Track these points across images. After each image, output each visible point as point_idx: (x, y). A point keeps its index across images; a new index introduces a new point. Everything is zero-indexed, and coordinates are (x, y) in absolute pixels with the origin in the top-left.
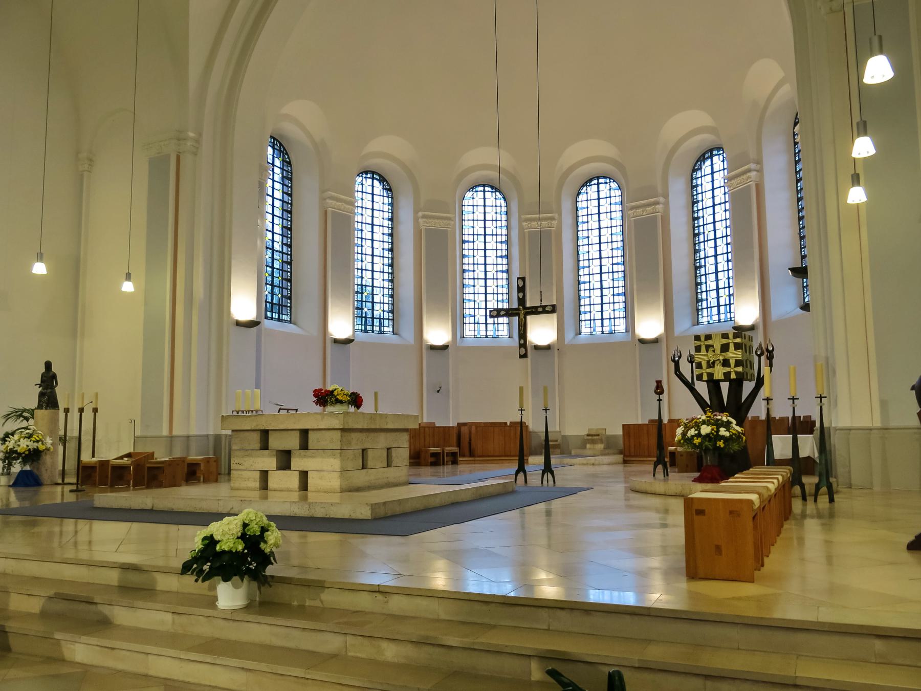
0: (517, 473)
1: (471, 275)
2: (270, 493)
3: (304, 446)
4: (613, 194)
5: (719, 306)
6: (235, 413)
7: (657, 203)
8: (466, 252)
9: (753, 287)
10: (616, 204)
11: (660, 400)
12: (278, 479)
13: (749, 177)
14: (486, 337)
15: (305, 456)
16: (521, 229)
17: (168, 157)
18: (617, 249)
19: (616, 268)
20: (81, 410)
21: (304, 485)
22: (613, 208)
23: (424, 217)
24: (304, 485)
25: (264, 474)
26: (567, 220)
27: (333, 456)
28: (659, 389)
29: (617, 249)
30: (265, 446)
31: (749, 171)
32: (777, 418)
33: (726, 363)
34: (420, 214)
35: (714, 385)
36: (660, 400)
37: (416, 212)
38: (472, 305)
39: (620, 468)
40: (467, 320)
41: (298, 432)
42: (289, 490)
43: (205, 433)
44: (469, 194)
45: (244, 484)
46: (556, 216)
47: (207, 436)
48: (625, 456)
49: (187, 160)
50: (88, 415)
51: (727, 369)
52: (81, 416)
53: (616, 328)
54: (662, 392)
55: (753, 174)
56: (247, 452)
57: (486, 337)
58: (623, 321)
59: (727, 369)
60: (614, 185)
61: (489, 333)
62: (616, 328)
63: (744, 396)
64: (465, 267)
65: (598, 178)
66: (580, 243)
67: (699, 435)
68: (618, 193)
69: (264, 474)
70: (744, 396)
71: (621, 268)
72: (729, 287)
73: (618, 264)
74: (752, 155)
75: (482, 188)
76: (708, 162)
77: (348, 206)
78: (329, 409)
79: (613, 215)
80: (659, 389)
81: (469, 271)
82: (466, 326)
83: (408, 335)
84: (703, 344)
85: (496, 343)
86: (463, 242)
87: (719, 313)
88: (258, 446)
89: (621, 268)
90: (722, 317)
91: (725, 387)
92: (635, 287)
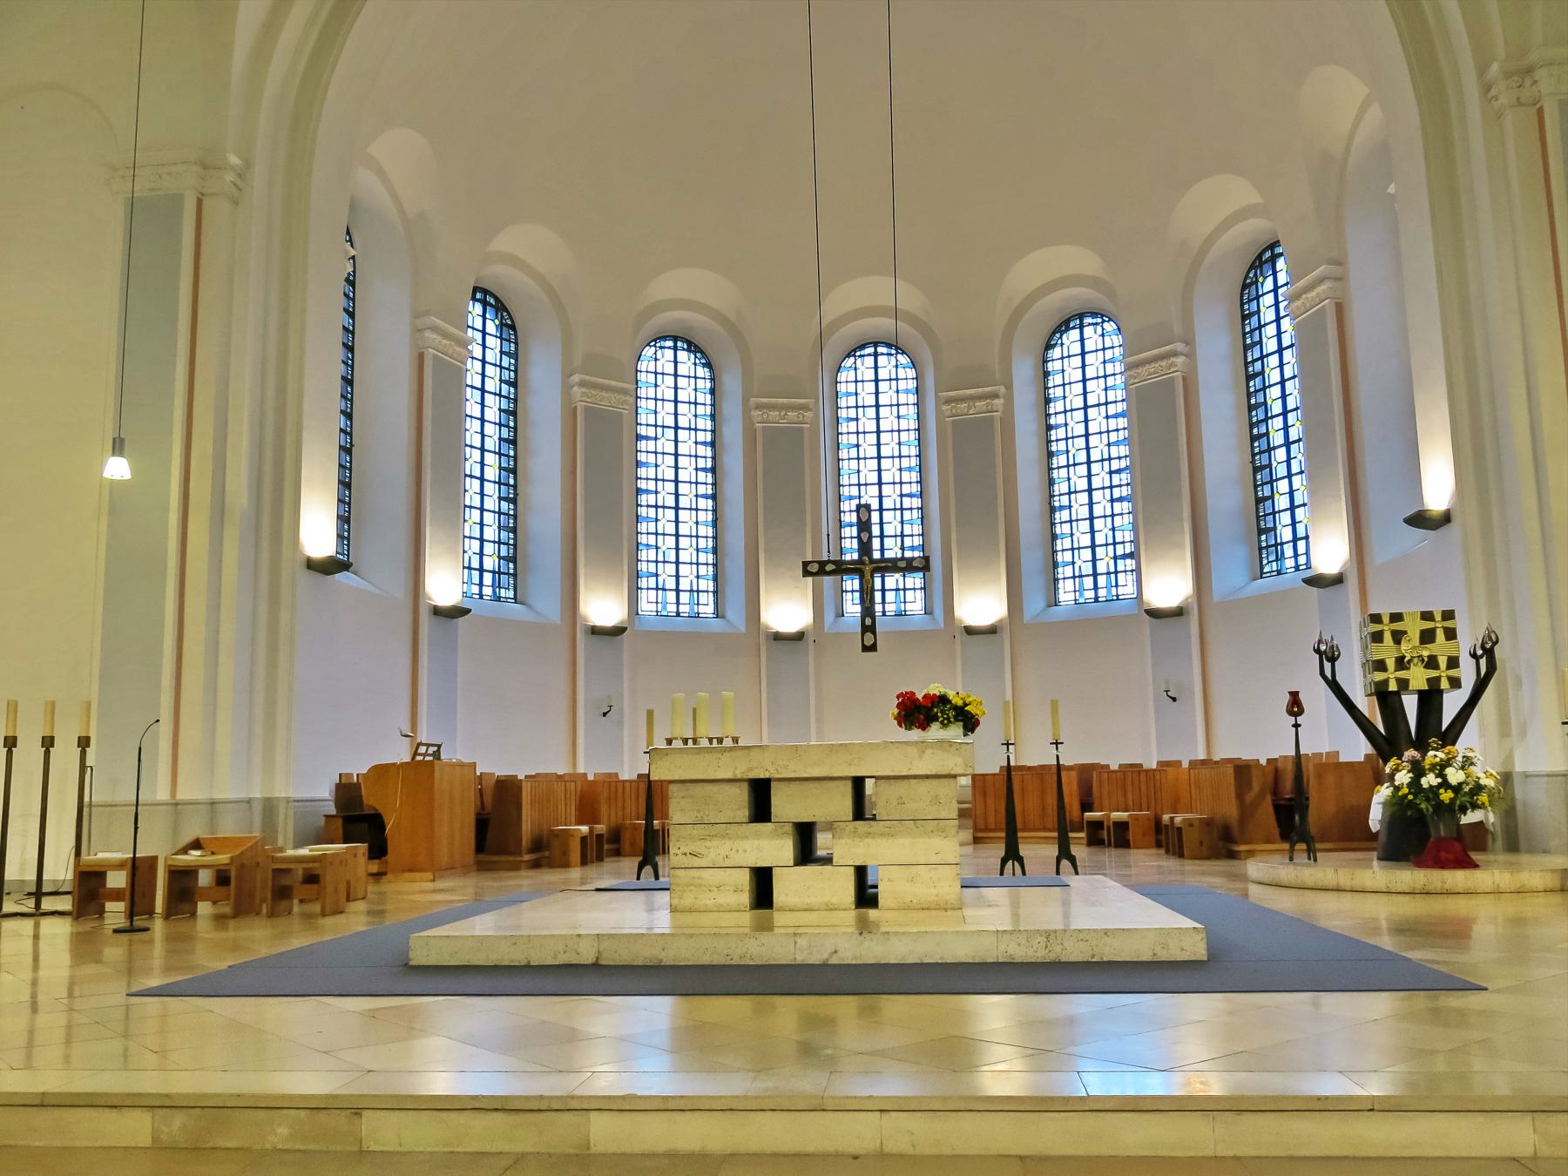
0: (1004, 862)
1: (651, 499)
2: (779, 918)
3: (860, 811)
4: (901, 374)
5: (1095, 575)
6: (677, 744)
7: (996, 396)
8: (642, 457)
9: (1181, 546)
10: (907, 391)
11: (1296, 726)
12: (791, 885)
13: (1173, 365)
14: (678, 614)
15: (868, 834)
16: (939, 415)
17: (177, 200)
18: (910, 469)
19: (907, 502)
20: (48, 742)
21: (866, 896)
22: (903, 398)
23: (582, 384)
24: (866, 896)
25: (762, 881)
26: (1024, 397)
27: (942, 832)
28: (1295, 706)
29: (910, 469)
30: (761, 810)
31: (1175, 354)
32: (1263, 762)
33: (1401, 663)
34: (576, 378)
35: (1387, 700)
36: (1296, 726)
37: (567, 374)
38: (652, 554)
39: (970, 849)
40: (643, 583)
41: (745, 786)
42: (830, 908)
43: (243, 795)
44: (649, 352)
45: (707, 900)
46: (1002, 389)
47: (249, 801)
48: (976, 829)
49: (217, 211)
50: (65, 756)
51: (1433, 673)
52: (47, 753)
53: (909, 606)
54: (1301, 712)
55: (1180, 360)
56: (711, 828)
57: (678, 614)
58: (920, 594)
59: (1433, 673)
60: (903, 359)
61: (682, 608)
62: (909, 606)
63: (1446, 721)
64: (642, 485)
65: (876, 345)
66: (843, 454)
67: (1445, 784)
68: (911, 373)
69: (762, 881)
70: (1446, 721)
71: (916, 502)
72: (1115, 544)
73: (910, 495)
74: (1178, 329)
75: (670, 343)
76: (1074, 334)
77: (458, 349)
78: (935, 732)
79: (903, 410)
80: (1295, 706)
81: (647, 492)
82: (643, 595)
83: (547, 604)
84: (1387, 628)
85: (695, 626)
86: (639, 437)
87: (1096, 588)
88: (744, 813)
89: (916, 502)
90: (1102, 593)
91: (1410, 703)
92: (954, 536)
